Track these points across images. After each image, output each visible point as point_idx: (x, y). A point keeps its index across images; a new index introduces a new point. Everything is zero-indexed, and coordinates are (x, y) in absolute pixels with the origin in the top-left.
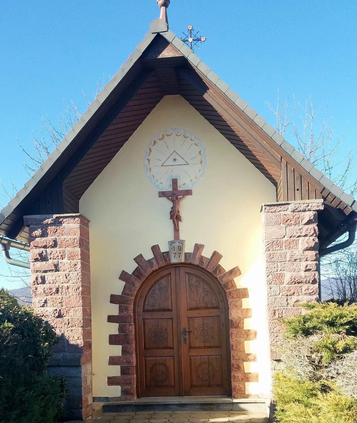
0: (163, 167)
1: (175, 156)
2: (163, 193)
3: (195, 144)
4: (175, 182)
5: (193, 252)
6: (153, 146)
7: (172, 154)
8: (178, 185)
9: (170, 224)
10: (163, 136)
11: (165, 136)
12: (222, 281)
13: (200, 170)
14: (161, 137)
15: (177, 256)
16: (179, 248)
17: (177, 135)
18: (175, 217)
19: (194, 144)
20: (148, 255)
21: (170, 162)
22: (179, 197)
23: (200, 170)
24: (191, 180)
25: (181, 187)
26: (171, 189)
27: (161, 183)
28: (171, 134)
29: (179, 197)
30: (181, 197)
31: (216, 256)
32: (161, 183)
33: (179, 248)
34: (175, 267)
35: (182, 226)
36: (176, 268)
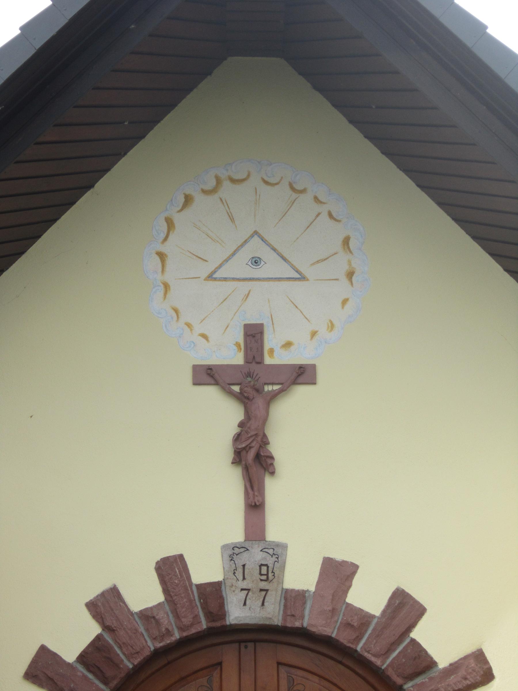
0: (211, 283)
1: (255, 248)
2: (211, 369)
3: (330, 215)
4: (254, 335)
5: (312, 589)
6: (179, 211)
7: (246, 242)
8: (267, 346)
9: (230, 485)
10: (219, 181)
11: (227, 184)
12: (169, 633)
13: (345, 302)
14: (212, 183)
15: (254, 602)
16: (264, 569)
17: (266, 183)
18: (253, 458)
19: (325, 215)
20: (144, 594)
21: (239, 267)
22: (268, 388)
23: (345, 302)
24: (314, 334)
25: (277, 354)
26: (239, 359)
27: (205, 337)
28: (244, 176)
29: (268, 388)
30: (276, 387)
31: (404, 609)
32: (205, 337)
33: (264, 569)
34: (240, 642)
35: (276, 490)
36: (243, 645)
